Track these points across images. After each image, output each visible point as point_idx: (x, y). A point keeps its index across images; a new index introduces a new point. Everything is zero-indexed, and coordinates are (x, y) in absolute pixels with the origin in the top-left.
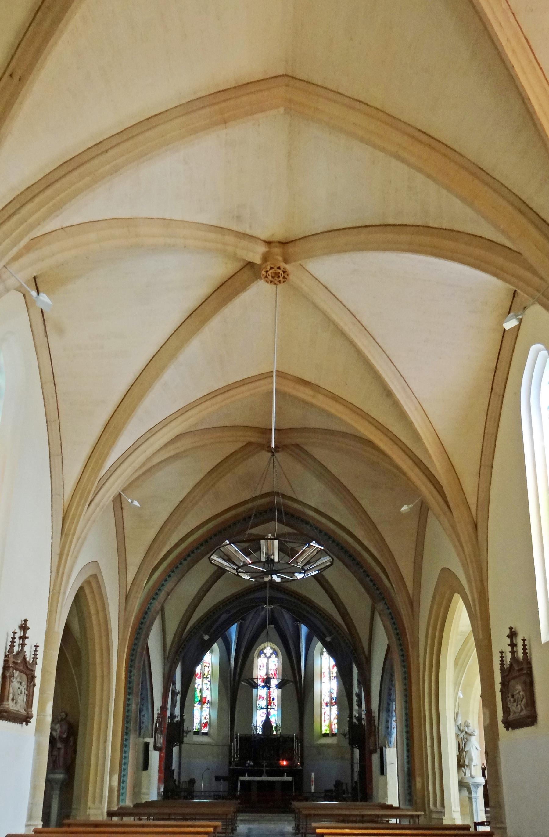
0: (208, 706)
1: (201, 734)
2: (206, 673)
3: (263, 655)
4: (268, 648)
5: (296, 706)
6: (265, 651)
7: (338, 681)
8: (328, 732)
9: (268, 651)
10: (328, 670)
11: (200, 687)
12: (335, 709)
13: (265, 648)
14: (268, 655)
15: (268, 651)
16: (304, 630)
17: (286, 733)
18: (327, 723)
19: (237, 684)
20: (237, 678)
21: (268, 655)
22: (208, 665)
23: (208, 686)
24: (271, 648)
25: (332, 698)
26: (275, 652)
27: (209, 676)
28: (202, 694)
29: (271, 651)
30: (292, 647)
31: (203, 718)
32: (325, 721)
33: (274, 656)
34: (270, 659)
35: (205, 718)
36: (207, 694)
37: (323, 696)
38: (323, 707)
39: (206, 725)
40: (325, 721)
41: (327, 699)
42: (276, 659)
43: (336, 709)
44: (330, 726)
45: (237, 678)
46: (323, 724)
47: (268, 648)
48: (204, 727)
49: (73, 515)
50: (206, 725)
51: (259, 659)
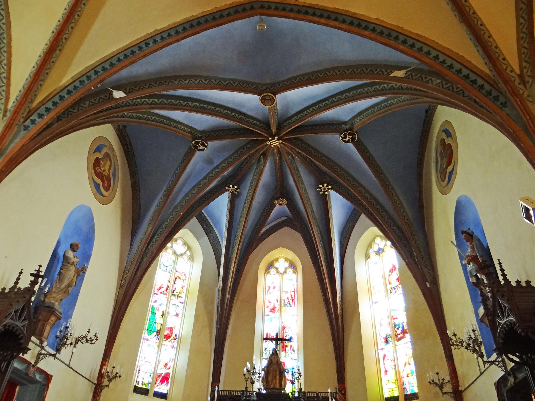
0: (175, 344)
1: (151, 393)
2: (178, 290)
3: (273, 271)
4: (282, 261)
5: (331, 347)
6: (276, 265)
7: (406, 293)
8: (396, 394)
9: (281, 265)
10: (382, 282)
11: (163, 308)
12: (405, 348)
13: (277, 260)
14: (281, 270)
15: (281, 265)
16: (338, 206)
17: (317, 388)
18: (392, 375)
19: (227, 303)
20: (228, 296)
21: (281, 270)
22: (183, 277)
23: (179, 311)
24: (286, 260)
25: (395, 326)
26: (292, 265)
27: (183, 295)
28: (165, 321)
29: (287, 265)
30: (317, 238)
31: (162, 365)
32: (386, 371)
33: (290, 271)
34: (285, 276)
35: (166, 365)
36: (172, 322)
37: (378, 327)
38: (380, 347)
39: (165, 379)
40: (386, 371)
41: (387, 330)
42: (294, 276)
43: (410, 345)
44: (399, 380)
45: (228, 296)
46: (385, 378)
47: (282, 261)
48: (162, 382)
49: (276, 379)
50: (165, 379)
51: (268, 276)
